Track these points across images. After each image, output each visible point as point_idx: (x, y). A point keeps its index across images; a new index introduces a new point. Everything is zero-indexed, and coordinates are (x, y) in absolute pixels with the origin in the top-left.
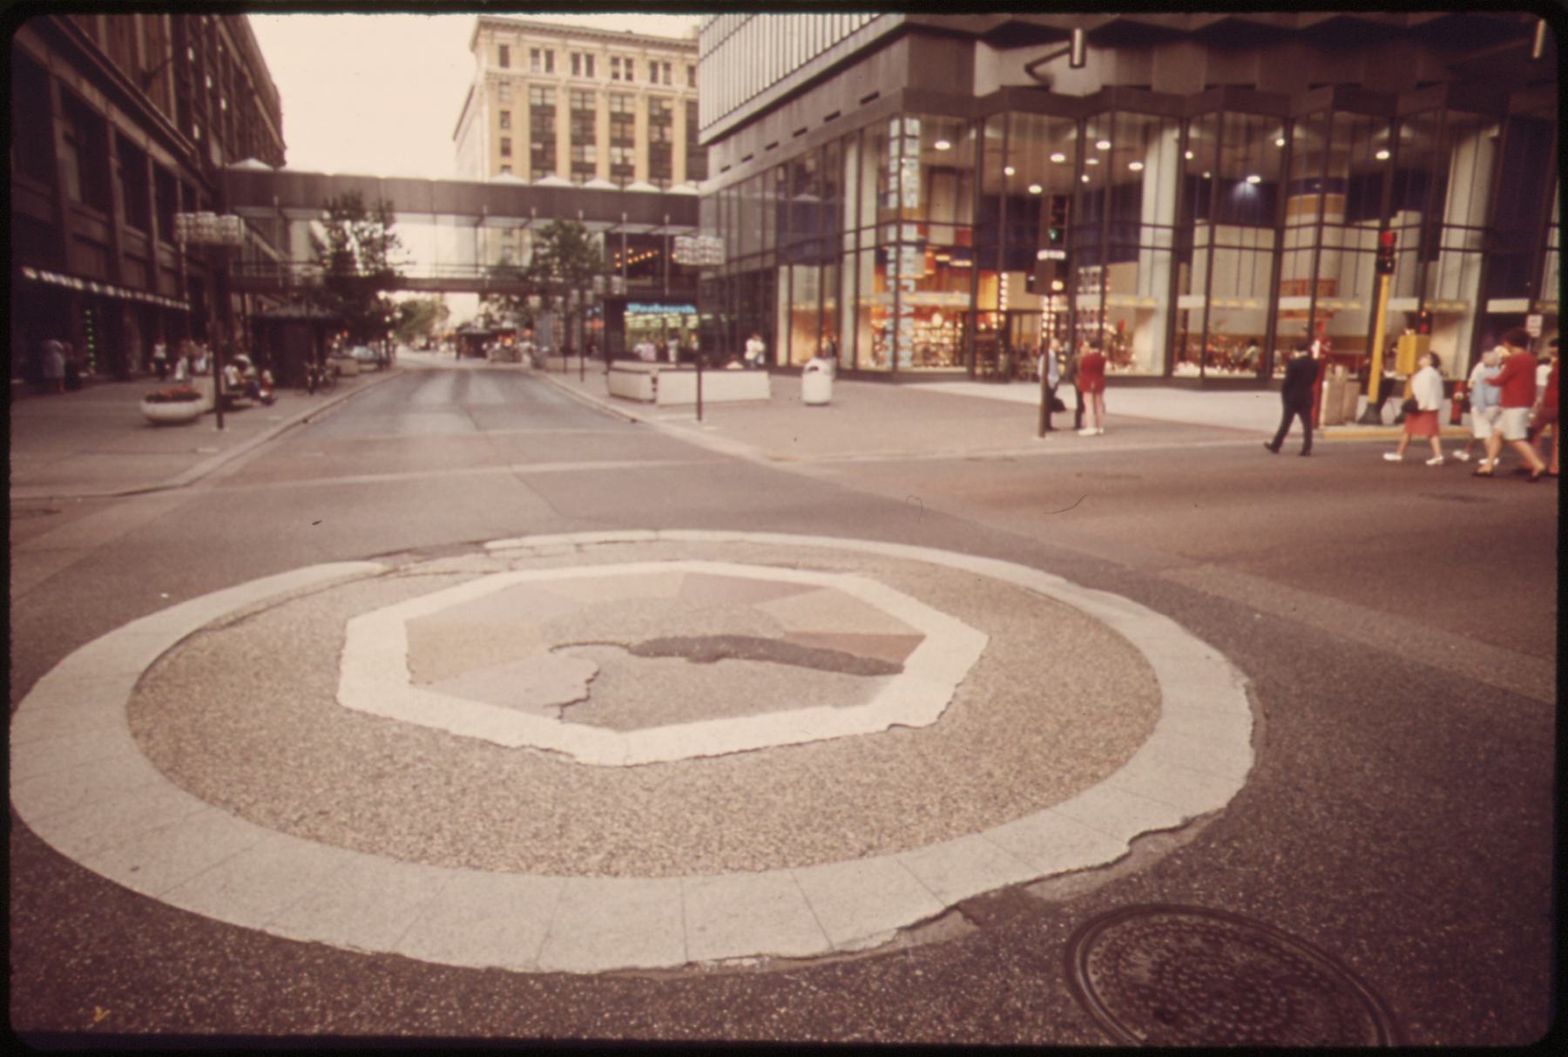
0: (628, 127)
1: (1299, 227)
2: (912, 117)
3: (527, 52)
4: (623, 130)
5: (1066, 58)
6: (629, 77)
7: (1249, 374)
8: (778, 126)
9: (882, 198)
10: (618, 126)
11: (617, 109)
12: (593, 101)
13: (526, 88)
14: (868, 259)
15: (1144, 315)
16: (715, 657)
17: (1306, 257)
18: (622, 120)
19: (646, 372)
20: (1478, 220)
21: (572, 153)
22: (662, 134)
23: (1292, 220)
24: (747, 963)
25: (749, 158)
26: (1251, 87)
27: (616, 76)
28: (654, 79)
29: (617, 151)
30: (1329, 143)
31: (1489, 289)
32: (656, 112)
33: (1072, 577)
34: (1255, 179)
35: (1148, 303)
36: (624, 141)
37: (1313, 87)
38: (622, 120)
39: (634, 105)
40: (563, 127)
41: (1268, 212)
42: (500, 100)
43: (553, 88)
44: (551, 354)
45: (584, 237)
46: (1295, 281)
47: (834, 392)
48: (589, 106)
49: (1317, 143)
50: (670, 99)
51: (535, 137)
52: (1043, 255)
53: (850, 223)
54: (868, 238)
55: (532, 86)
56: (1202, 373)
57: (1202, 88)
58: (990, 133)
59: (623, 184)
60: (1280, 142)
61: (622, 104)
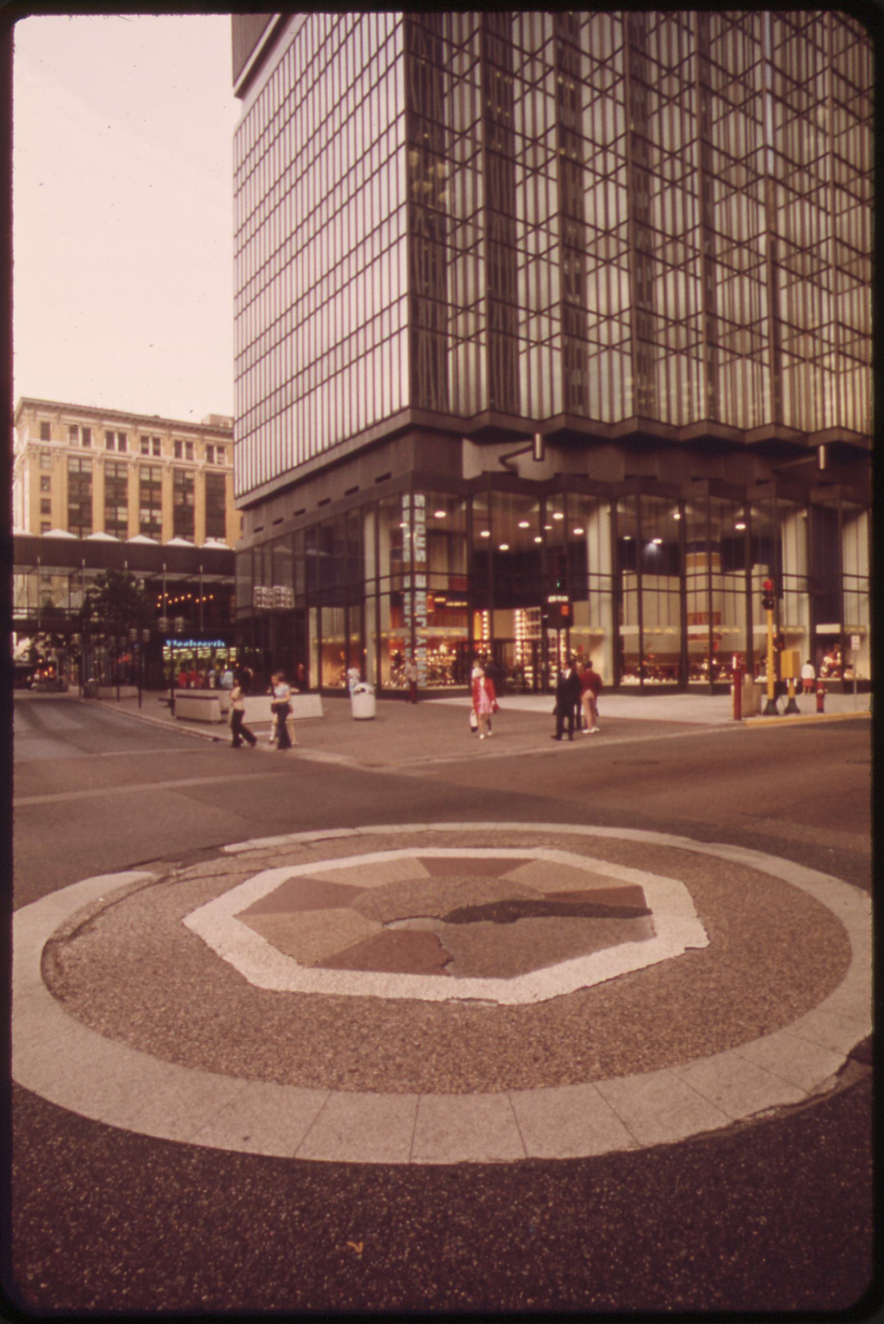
0: (155, 493)
1: (695, 575)
2: (418, 493)
3: (66, 429)
4: (151, 495)
5: (529, 454)
6: (157, 452)
7: (673, 682)
8: (306, 500)
9: (396, 553)
10: (147, 492)
11: (146, 477)
12: (126, 471)
13: (65, 458)
14: (385, 601)
15: (596, 641)
16: (513, 918)
17: (702, 597)
18: (150, 487)
19: (216, 698)
20: (803, 572)
21: (106, 513)
22: (185, 499)
23: (690, 570)
24: (771, 1113)
25: (280, 521)
26: (654, 478)
27: (145, 451)
28: (178, 454)
29: (146, 512)
30: (709, 519)
31: (817, 617)
32: (180, 481)
33: (694, 836)
34: (658, 541)
35: (599, 632)
36: (155, 505)
37: (695, 480)
38: (150, 487)
39: (161, 475)
40: (98, 492)
41: (672, 562)
42: (41, 467)
43: (89, 459)
44: (102, 684)
45: (134, 584)
46: (696, 614)
47: (378, 707)
48: (122, 475)
49: (701, 518)
50: (192, 471)
51: (71, 499)
52: (552, 599)
53: (370, 573)
54: (385, 586)
55: (70, 457)
56: (642, 682)
57: (622, 479)
58: (476, 506)
59: (81, 534)
60: (677, 516)
61: (151, 474)
